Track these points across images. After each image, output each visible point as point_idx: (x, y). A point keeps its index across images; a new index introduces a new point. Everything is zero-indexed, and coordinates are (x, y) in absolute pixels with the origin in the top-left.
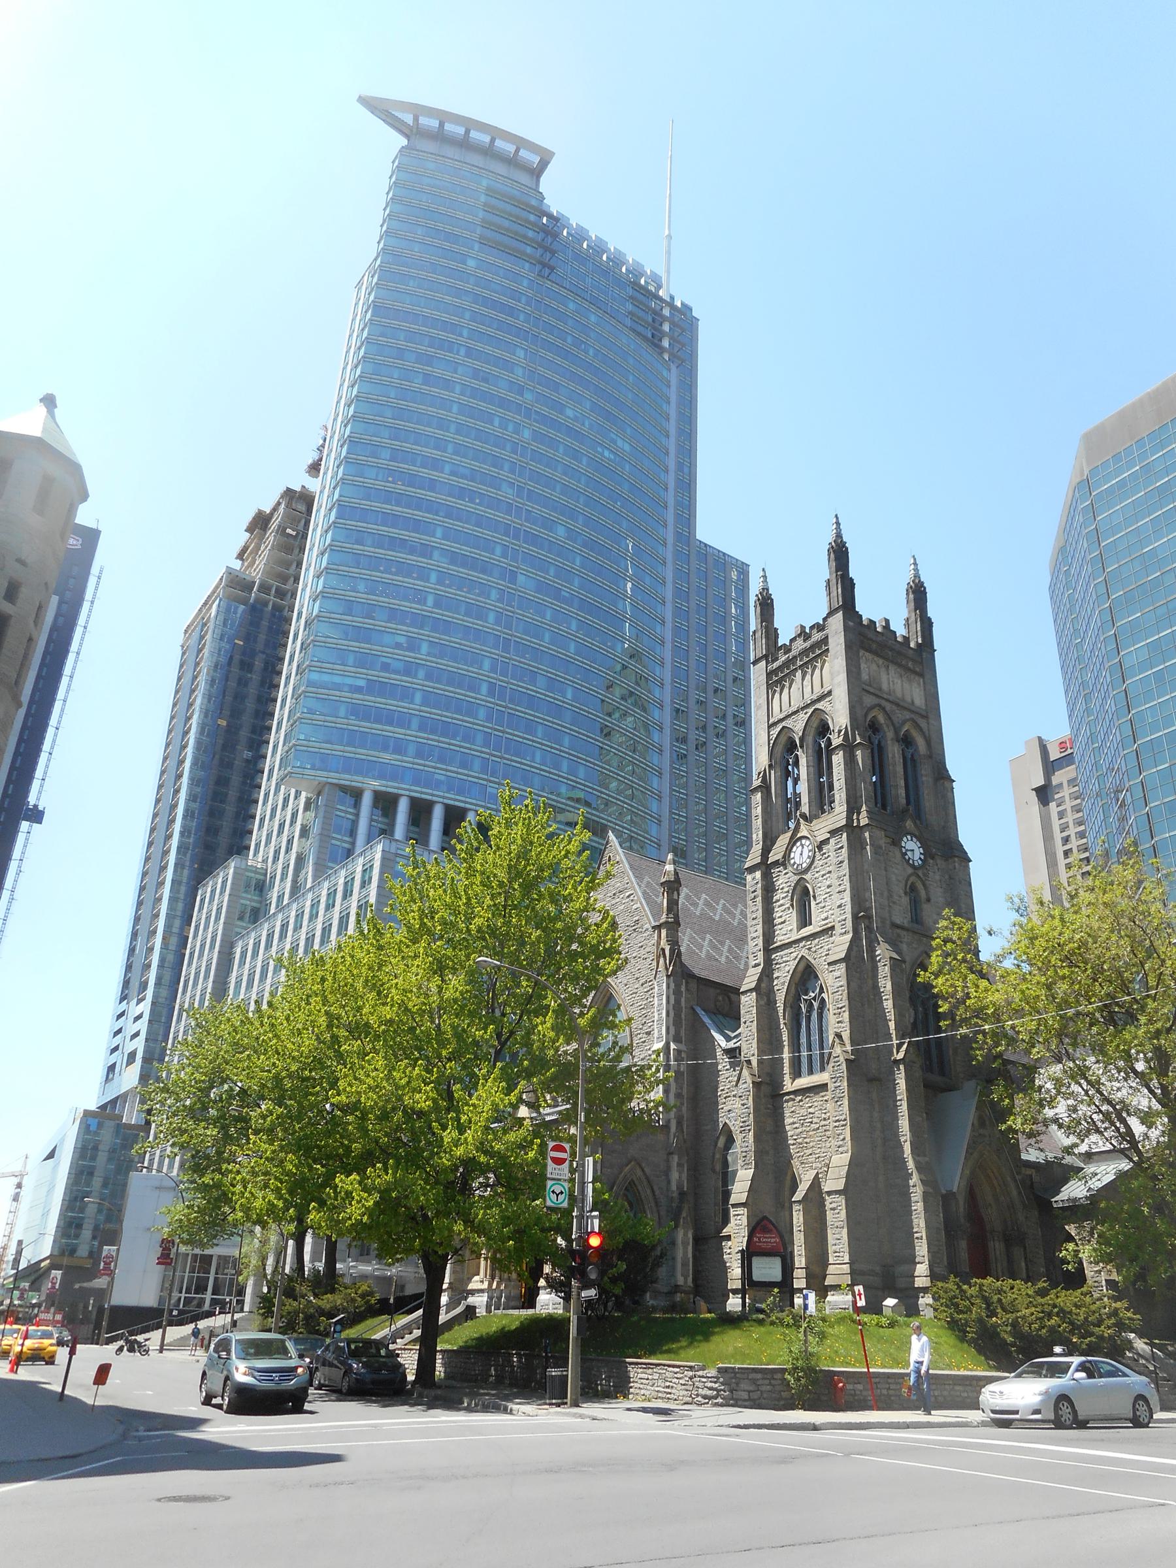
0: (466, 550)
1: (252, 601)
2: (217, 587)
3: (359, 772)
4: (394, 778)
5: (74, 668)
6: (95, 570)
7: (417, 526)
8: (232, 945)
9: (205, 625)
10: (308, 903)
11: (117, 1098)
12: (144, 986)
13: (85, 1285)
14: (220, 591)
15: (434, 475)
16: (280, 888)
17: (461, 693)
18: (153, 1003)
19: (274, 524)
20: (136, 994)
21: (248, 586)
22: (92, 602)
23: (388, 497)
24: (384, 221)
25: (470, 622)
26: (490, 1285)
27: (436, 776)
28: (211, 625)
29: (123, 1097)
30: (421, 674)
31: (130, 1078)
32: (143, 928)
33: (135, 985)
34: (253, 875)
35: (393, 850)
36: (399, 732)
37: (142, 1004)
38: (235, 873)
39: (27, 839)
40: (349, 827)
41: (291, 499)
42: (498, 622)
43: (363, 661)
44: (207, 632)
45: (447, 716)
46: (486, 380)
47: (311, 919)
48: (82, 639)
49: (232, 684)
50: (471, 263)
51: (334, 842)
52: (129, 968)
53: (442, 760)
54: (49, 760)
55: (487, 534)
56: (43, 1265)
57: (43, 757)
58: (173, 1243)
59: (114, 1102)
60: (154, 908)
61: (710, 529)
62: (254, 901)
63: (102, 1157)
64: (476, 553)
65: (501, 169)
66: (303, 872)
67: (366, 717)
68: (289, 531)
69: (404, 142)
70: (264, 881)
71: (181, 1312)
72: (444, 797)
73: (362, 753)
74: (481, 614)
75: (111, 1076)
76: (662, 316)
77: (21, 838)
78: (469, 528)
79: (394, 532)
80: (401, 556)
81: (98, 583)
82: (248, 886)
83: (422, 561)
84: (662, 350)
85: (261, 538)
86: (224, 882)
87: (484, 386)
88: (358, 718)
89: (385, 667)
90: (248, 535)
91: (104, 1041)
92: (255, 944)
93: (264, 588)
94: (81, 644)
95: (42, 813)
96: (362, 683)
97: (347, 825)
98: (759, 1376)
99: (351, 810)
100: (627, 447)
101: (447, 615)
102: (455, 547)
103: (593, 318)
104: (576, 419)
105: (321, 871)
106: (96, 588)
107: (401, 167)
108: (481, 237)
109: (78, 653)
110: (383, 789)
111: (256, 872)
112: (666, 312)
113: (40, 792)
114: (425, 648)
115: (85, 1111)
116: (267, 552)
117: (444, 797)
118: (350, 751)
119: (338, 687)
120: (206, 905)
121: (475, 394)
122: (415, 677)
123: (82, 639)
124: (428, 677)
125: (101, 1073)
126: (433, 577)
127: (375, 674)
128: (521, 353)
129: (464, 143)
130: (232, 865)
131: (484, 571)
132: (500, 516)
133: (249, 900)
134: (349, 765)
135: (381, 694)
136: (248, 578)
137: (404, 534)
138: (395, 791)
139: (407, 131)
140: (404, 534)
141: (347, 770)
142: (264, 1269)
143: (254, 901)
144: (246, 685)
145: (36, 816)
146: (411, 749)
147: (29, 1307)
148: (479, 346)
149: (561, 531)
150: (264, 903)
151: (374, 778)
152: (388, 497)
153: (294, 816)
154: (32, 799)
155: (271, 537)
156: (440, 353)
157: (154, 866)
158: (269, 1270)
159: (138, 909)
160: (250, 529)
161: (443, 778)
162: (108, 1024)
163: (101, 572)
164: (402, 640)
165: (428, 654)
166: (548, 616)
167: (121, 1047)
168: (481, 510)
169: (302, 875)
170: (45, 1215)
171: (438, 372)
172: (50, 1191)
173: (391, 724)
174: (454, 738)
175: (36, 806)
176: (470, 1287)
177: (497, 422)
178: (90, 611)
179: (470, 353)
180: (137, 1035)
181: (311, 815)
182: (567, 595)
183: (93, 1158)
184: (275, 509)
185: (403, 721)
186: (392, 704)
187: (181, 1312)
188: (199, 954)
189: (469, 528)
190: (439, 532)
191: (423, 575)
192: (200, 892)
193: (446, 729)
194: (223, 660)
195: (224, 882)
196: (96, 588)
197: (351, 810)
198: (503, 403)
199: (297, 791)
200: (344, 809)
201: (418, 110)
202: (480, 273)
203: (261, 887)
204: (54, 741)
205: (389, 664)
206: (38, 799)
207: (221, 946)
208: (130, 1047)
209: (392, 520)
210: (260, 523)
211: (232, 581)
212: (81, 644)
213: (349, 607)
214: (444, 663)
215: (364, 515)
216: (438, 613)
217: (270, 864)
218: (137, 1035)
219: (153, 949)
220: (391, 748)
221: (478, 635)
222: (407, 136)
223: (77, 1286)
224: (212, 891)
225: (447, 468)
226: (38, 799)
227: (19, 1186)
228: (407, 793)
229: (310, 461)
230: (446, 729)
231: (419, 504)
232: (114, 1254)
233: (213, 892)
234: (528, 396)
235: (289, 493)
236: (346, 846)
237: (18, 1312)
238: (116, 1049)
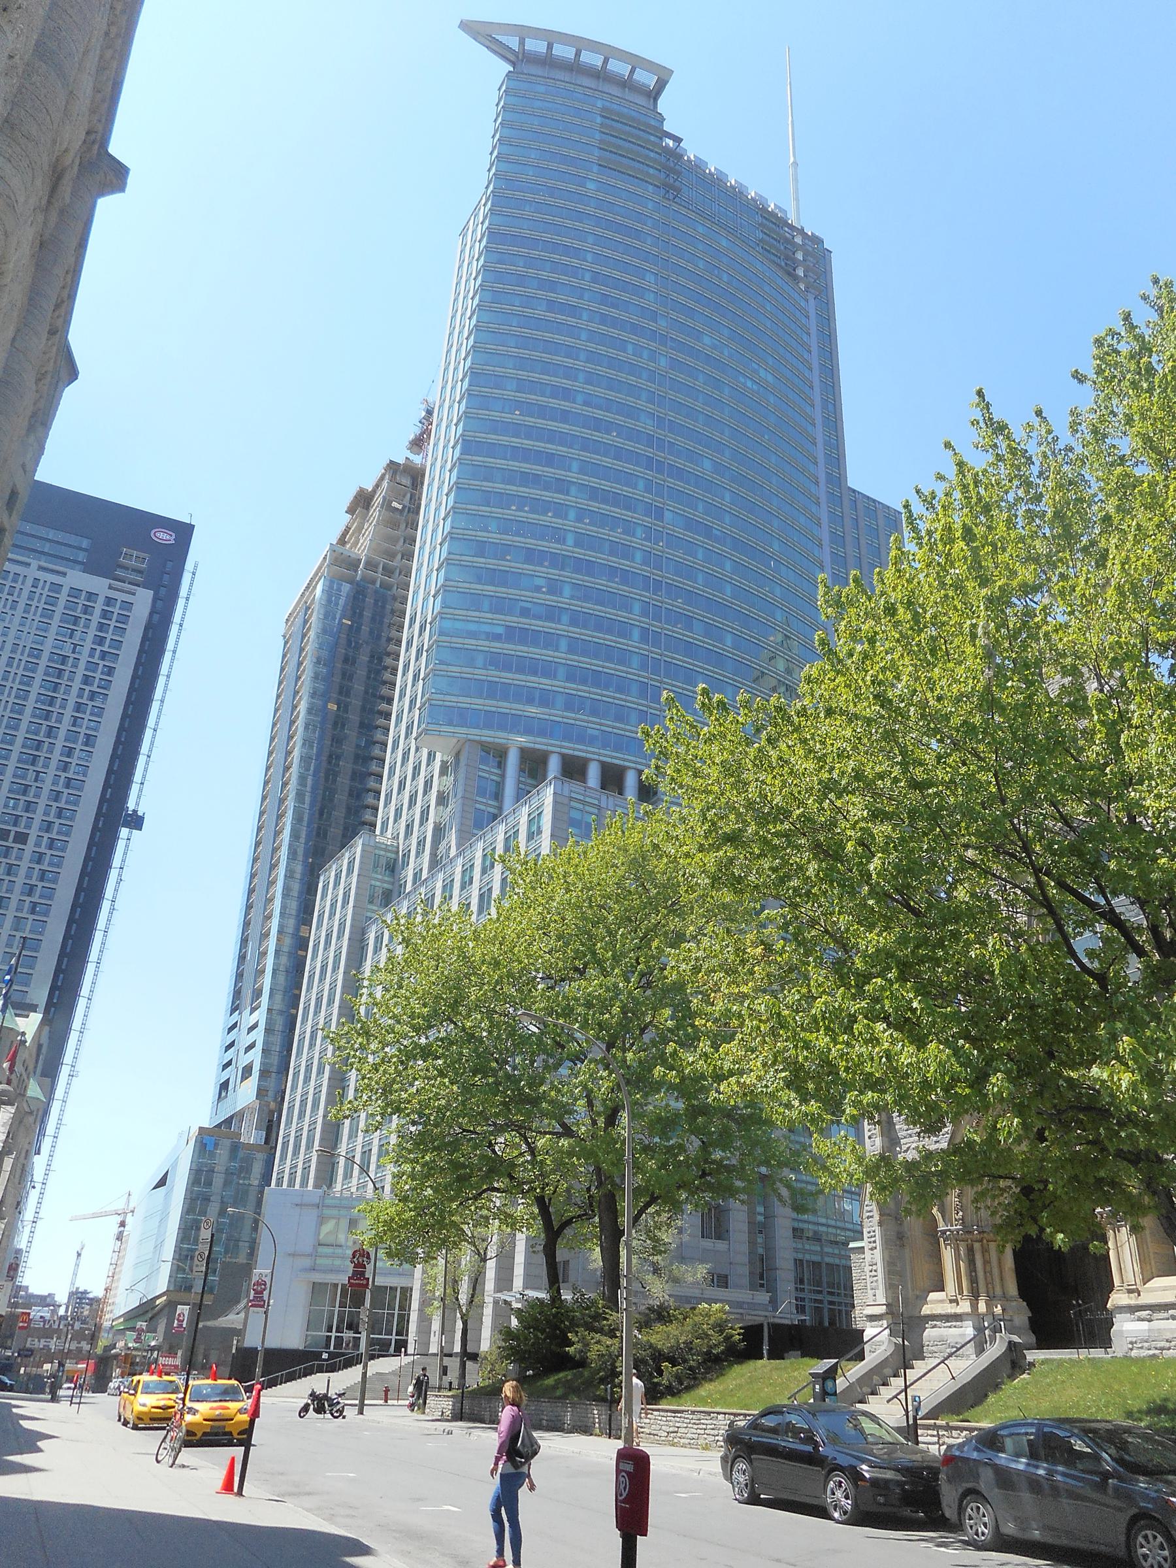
0: (605, 485)
1: (358, 578)
2: (320, 568)
3: (502, 727)
4: (542, 733)
5: (171, 667)
6: (189, 566)
7: (550, 460)
8: (363, 932)
9: (308, 608)
10: (459, 870)
11: (232, 1117)
12: (258, 994)
13: (209, 1323)
14: (325, 570)
15: (565, 405)
16: (416, 864)
17: (609, 639)
18: (269, 1010)
19: (378, 500)
20: (249, 1001)
21: (353, 564)
22: (187, 599)
23: (516, 430)
24: (492, 165)
25: (614, 561)
26: (975, 1306)
27: (590, 731)
28: (316, 606)
29: (240, 1115)
30: (565, 618)
31: (246, 1094)
32: (254, 932)
33: (247, 994)
34: (382, 853)
35: (566, 793)
36: (545, 683)
37: (257, 1013)
38: (363, 850)
39: (127, 846)
40: (494, 789)
41: (395, 473)
42: (645, 562)
43: (500, 606)
44: (311, 615)
45: (596, 664)
46: (613, 306)
47: (463, 888)
48: (178, 637)
49: (337, 679)
50: (591, 185)
51: (478, 806)
52: (239, 976)
53: (594, 712)
54: (147, 763)
55: (629, 468)
56: (158, 1302)
57: (148, 733)
58: (369, 1257)
59: (228, 1122)
60: (265, 909)
61: (851, 483)
62: (385, 882)
63: (218, 1180)
64: (617, 488)
65: (615, 91)
66: (444, 843)
67: (507, 667)
68: (395, 504)
70: (396, 860)
71: (332, 1356)
72: (599, 755)
73: (505, 706)
74: (626, 552)
75: (223, 1094)
76: (794, 244)
77: (121, 845)
78: (607, 461)
79: (526, 467)
80: (535, 493)
81: (193, 579)
82: (376, 866)
83: (559, 498)
84: (795, 278)
85: (364, 518)
86: (351, 863)
87: (614, 312)
88: (497, 668)
89: (525, 612)
90: (349, 516)
91: (214, 1056)
92: (377, 937)
93: (371, 565)
94: (177, 643)
95: (142, 819)
96: (500, 630)
97: (491, 788)
99: (495, 771)
100: (770, 378)
101: (590, 555)
102: (594, 482)
103: (724, 243)
104: (714, 347)
105: (465, 839)
106: (191, 584)
108: (600, 158)
109: (174, 652)
110: (532, 745)
111: (386, 850)
112: (798, 240)
113: (139, 797)
114: (567, 591)
115: (200, 1128)
116: (372, 528)
117: (599, 755)
118: (490, 705)
119: (473, 635)
120: (330, 891)
121: (604, 319)
122: (559, 622)
123: (178, 637)
124: (574, 622)
125: (212, 1091)
126: (572, 514)
127: (514, 620)
128: (650, 278)
129: (575, 67)
130: (358, 845)
131: (628, 508)
132: (640, 448)
133: (380, 881)
134: (490, 720)
135: (523, 641)
136: (353, 556)
137: (537, 469)
138: (545, 747)
139: (513, 58)
140: (537, 469)
141: (488, 726)
142: (457, 1299)
143: (385, 882)
144: (351, 678)
145: (136, 822)
146: (560, 700)
147: (147, 1351)
148: (606, 271)
149: (707, 464)
150: (397, 885)
151: (521, 734)
152: (516, 430)
153: (428, 785)
154: (131, 805)
155: (375, 512)
156: (564, 279)
157: (263, 865)
158: (463, 1298)
159: (247, 914)
160: (351, 511)
161: (596, 733)
162: (218, 1038)
163: (196, 567)
164: (540, 582)
165: (572, 597)
166: (700, 556)
167: (234, 1062)
168: (620, 442)
169: (442, 847)
170: (159, 1247)
171: (562, 299)
172: (163, 1219)
173: (535, 673)
174: (606, 688)
175: (135, 811)
176: (926, 1310)
177: (630, 348)
178: (186, 607)
179: (596, 277)
180: (251, 1046)
181: (449, 780)
182: (718, 533)
183: (209, 1184)
184: (377, 486)
185: (548, 671)
186: (535, 652)
187: (332, 1356)
188: (339, 932)
189: (607, 461)
190: (575, 466)
191: (560, 511)
192: (322, 878)
193: (597, 679)
194: (325, 654)
195: (351, 863)
196: (191, 584)
197: (495, 771)
198: (635, 329)
199: (429, 754)
200: (489, 771)
201: (523, 32)
202: (601, 196)
203: (393, 867)
204: (152, 743)
205: (529, 610)
206: (137, 804)
207: (351, 933)
208: (244, 1060)
209: (525, 455)
210: (362, 501)
211: (336, 559)
212: (177, 643)
213: (481, 548)
214: (589, 607)
215: (491, 450)
216: (579, 553)
217: (401, 841)
218: (251, 1046)
219: (266, 953)
220: (537, 701)
221: (626, 577)
222: (513, 64)
224: (336, 875)
225: (580, 398)
226: (137, 804)
227: (123, 1224)
228: (558, 750)
229: (412, 437)
230: (597, 679)
231: (552, 437)
232: (268, 1280)
234: (663, 323)
235: (392, 467)
236: (492, 810)
237: (135, 1356)
238: (229, 1064)
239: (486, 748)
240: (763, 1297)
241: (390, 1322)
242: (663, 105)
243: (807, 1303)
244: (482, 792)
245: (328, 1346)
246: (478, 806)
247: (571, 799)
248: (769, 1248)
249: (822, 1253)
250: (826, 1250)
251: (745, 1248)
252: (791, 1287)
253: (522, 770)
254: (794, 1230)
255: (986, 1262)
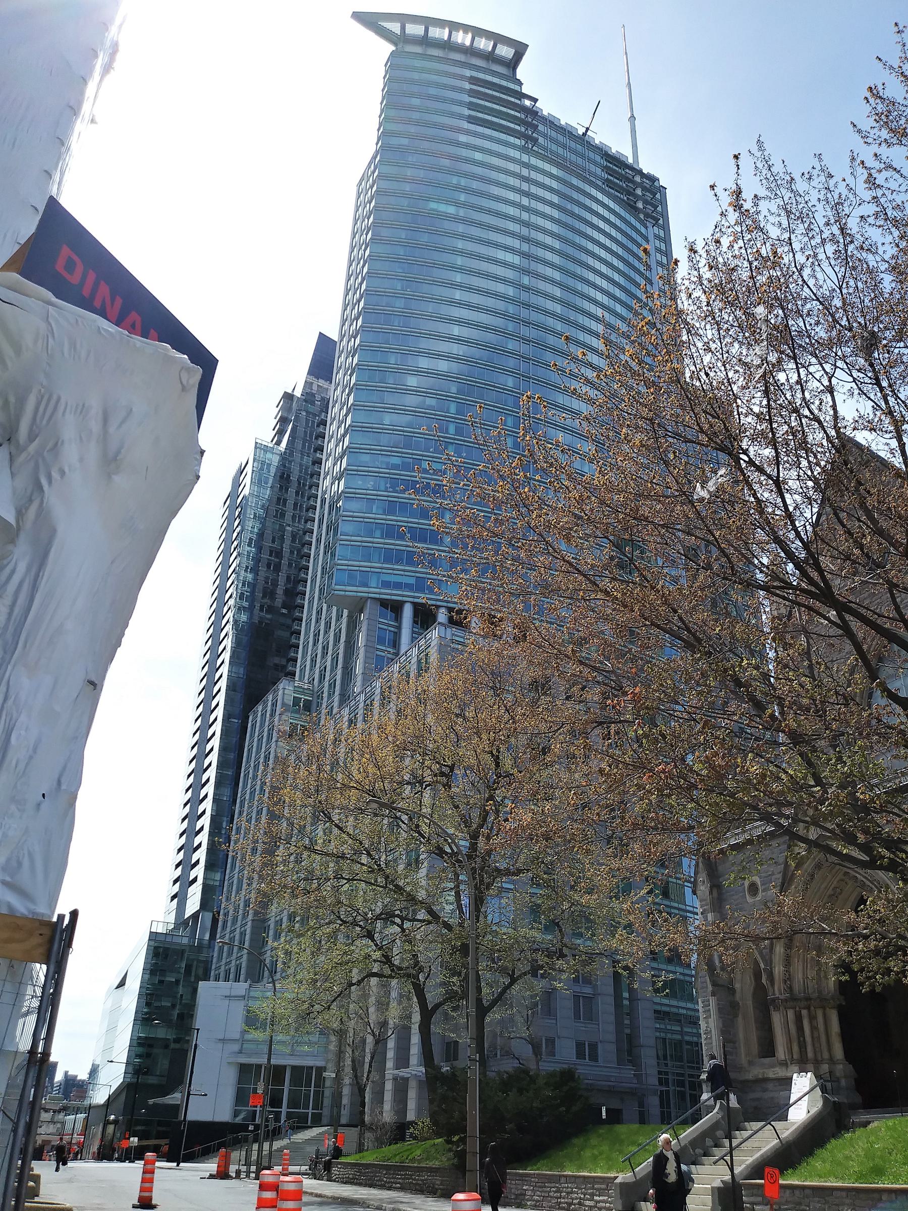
51: (378, 653)
69: (392, 48)
98: (844, 1194)
107: (394, 65)
200: (387, 621)
201: (404, 19)
222: (395, 44)
223: (151, 1102)
233: (263, 715)
239: (384, 603)
240: (628, 1072)
241: (307, 1096)
242: (521, 72)
243: (670, 1077)
244: (381, 641)
245: (254, 1119)
246: (378, 653)
247: (452, 641)
248: (634, 1026)
249: (682, 1033)
250: (686, 1029)
251: (612, 1028)
252: (654, 1062)
253: (415, 622)
254: (656, 1011)
255: (814, 1028)
